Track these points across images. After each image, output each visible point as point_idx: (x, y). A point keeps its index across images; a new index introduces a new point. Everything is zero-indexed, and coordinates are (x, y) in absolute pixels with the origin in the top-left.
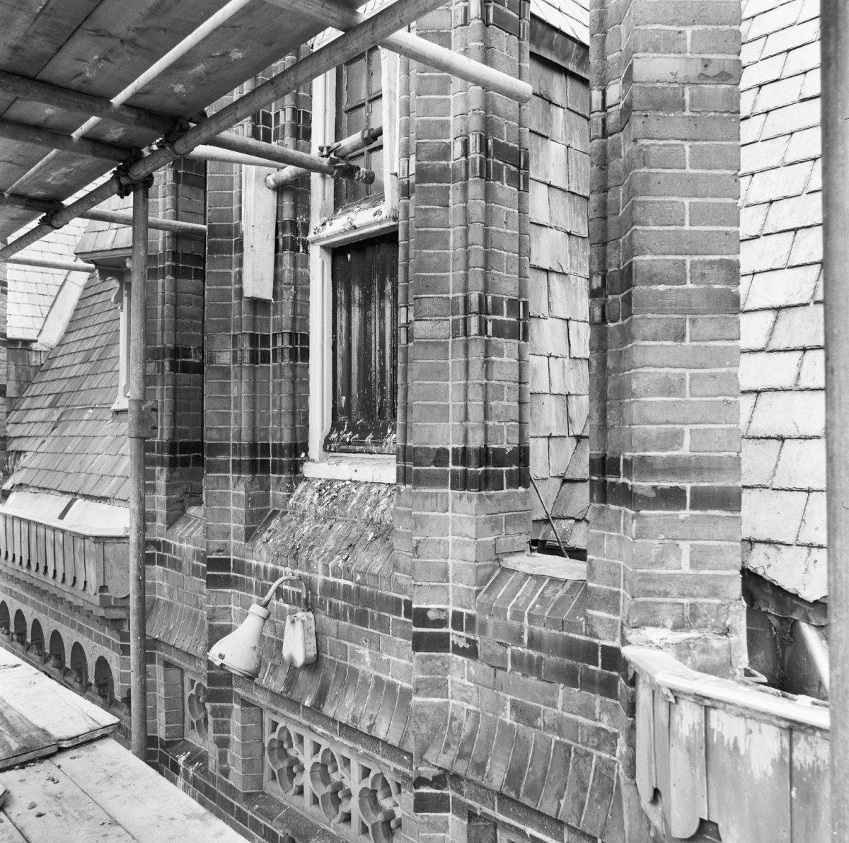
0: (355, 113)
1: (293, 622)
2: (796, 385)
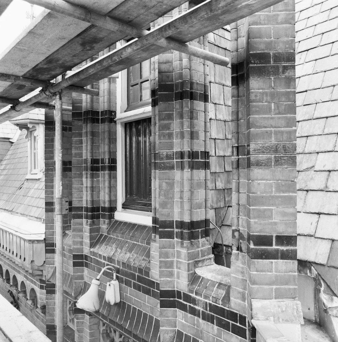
0: (39, 217)
1: (110, 285)
2: (327, 187)
